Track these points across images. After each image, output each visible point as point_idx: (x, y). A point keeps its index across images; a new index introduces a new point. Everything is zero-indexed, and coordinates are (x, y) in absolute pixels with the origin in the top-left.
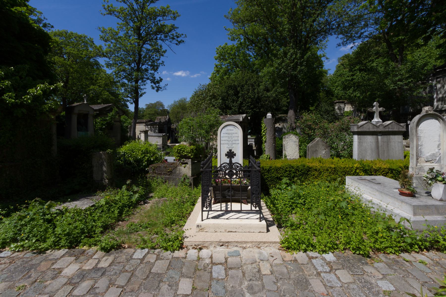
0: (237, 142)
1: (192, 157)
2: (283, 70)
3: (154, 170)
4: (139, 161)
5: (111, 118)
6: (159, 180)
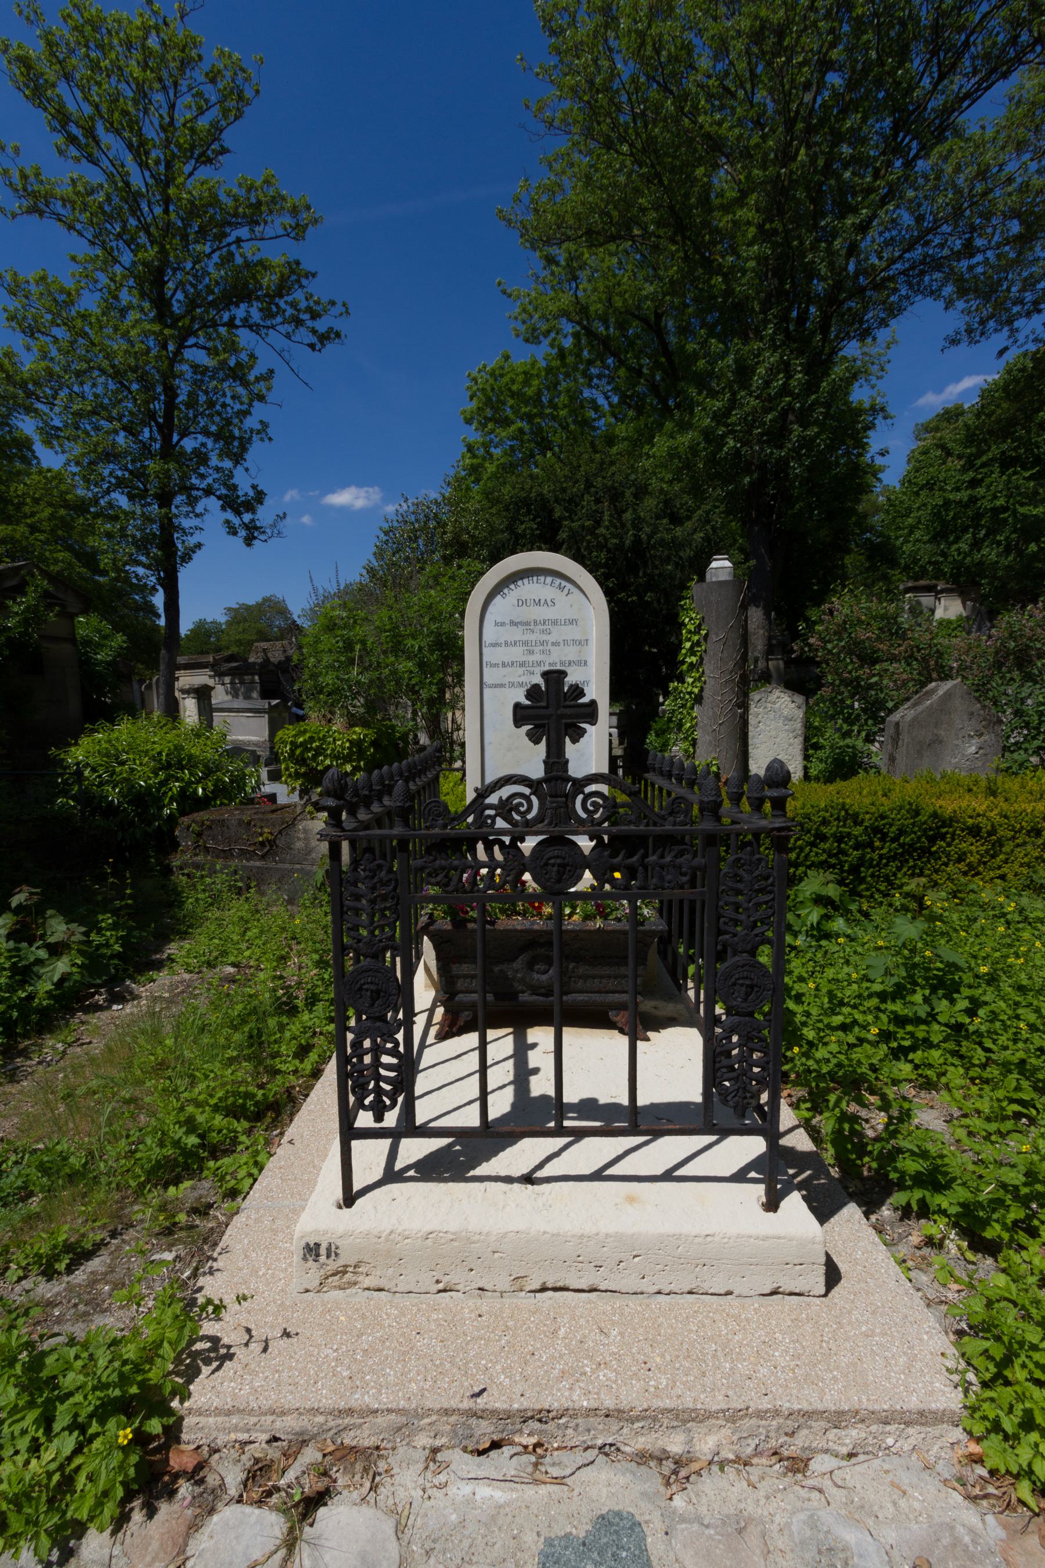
2: (731, 443)
3: (199, 835)
4: (144, 800)
5: (26, 622)
6: (220, 881)
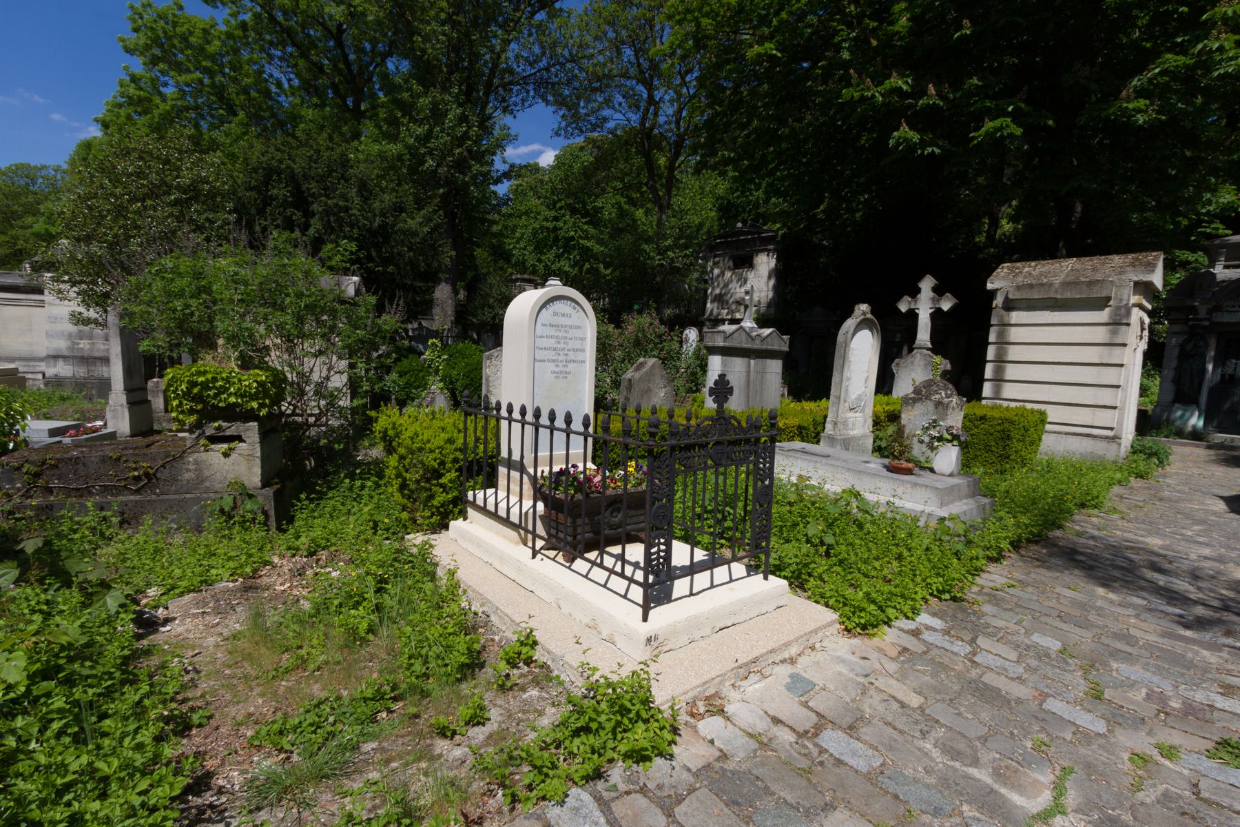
0: (580, 356)
1: (264, 412)
